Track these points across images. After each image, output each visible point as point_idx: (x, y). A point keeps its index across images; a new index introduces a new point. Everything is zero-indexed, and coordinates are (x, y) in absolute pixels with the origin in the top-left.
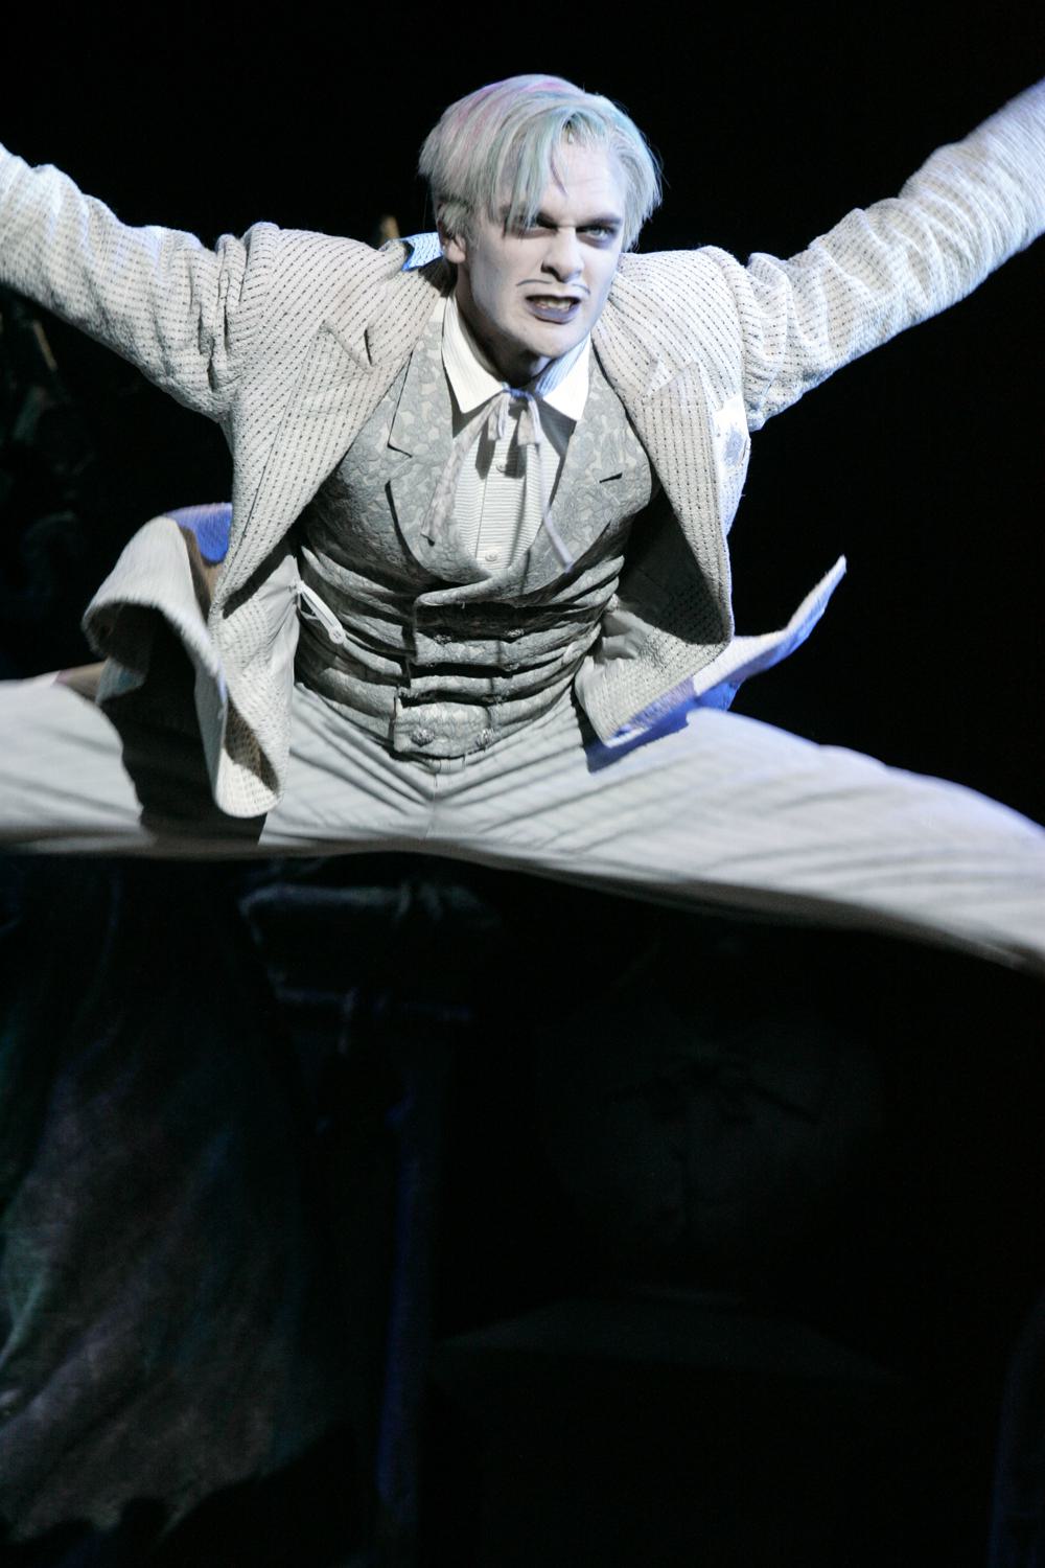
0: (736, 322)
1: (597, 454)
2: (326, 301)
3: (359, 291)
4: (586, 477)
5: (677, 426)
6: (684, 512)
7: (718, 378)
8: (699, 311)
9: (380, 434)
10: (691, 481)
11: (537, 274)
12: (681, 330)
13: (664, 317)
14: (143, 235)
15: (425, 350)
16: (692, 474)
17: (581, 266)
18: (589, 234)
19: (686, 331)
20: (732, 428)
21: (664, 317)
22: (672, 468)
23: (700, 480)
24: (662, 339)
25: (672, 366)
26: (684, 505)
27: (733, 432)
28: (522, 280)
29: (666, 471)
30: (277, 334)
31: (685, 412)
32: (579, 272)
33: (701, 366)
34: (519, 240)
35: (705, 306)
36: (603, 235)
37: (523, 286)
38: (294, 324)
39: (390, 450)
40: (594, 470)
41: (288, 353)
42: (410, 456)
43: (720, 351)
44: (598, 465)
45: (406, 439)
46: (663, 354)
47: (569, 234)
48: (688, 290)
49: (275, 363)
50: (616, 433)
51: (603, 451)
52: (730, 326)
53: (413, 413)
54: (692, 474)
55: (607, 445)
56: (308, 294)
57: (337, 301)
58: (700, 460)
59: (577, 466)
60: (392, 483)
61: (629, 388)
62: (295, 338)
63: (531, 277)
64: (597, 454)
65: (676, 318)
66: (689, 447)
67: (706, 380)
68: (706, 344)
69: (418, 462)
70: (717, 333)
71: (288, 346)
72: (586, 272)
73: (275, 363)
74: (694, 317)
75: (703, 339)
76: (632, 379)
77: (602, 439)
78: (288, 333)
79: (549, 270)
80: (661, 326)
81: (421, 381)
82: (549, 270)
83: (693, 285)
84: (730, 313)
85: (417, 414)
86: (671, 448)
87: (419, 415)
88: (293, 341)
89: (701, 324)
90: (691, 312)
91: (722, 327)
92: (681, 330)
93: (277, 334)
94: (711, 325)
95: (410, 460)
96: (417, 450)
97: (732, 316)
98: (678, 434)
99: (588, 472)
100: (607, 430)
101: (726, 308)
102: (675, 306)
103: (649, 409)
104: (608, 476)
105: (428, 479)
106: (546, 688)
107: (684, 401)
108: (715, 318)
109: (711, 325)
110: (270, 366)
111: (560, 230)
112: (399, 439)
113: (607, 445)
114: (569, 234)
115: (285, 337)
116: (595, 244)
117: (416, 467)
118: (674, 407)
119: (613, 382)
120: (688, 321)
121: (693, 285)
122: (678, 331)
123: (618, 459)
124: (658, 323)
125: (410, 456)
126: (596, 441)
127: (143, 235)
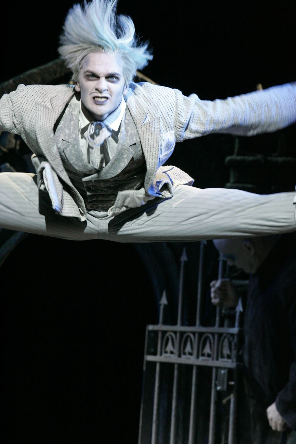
0: (175, 109)
1: (128, 138)
2: (39, 97)
3: (48, 93)
4: (125, 145)
5: (150, 134)
6: (148, 160)
7: (167, 125)
8: (163, 104)
9: (60, 136)
10: (151, 151)
11: (94, 90)
12: (156, 108)
13: (152, 103)
14: (164, 88)
15: (72, 111)
16: (152, 148)
17: (107, 88)
18: (110, 79)
19: (158, 108)
20: (169, 140)
21: (152, 103)
22: (147, 146)
23: (154, 151)
24: (150, 109)
25: (151, 117)
26: (148, 158)
27: (169, 141)
28: (90, 93)
29: (145, 147)
30: (26, 107)
31: (153, 130)
32: (105, 90)
33: (161, 119)
34: (226, 101)
35: (166, 103)
36: (115, 79)
37: (91, 95)
38: (30, 104)
39: (63, 141)
40: (127, 143)
41: (30, 113)
42: (68, 142)
43: (167, 116)
44: (128, 141)
45: (67, 137)
46: (149, 113)
47: (103, 80)
48: (162, 97)
49: (27, 116)
50: (133, 132)
51: (129, 137)
52: (172, 110)
53: (69, 130)
54: (152, 148)
55: (130, 135)
56: (34, 96)
57: (42, 96)
58: (155, 145)
59: (122, 142)
60: (64, 150)
61: (138, 121)
62: (31, 108)
63: (93, 91)
64: (128, 138)
65: (155, 104)
66: (152, 141)
67: (162, 124)
68: (163, 113)
69: (70, 144)
70: (167, 111)
71: (30, 111)
72: (109, 90)
73: (27, 116)
74: (161, 105)
75: (163, 112)
76: (139, 118)
77: (129, 134)
78: (29, 107)
79: (97, 89)
80: (150, 106)
81: (71, 121)
82: (97, 89)
83: (164, 97)
84: (173, 106)
85: (69, 130)
86: (147, 140)
87: (70, 131)
88: (31, 109)
89: (163, 108)
90: (161, 103)
91: (170, 110)
92: (156, 108)
93: (26, 107)
94: (166, 108)
95: (68, 143)
96: (70, 140)
97: (174, 108)
98: (150, 136)
99: (125, 144)
100: (130, 131)
101: (172, 104)
102: (156, 101)
103: (143, 127)
104: (131, 144)
105: (74, 149)
106: (114, 177)
107: (153, 127)
108: (168, 106)
109: (166, 108)
110: (26, 118)
111: (101, 78)
112: (65, 137)
113: (130, 135)
114: (103, 80)
115: (29, 108)
116: (113, 82)
117: (71, 146)
118: (150, 128)
119: (134, 118)
120: (159, 106)
121: (164, 97)
122: (155, 108)
123: (134, 139)
124: (149, 104)
125: (68, 142)
126: (127, 135)
127: (164, 88)
